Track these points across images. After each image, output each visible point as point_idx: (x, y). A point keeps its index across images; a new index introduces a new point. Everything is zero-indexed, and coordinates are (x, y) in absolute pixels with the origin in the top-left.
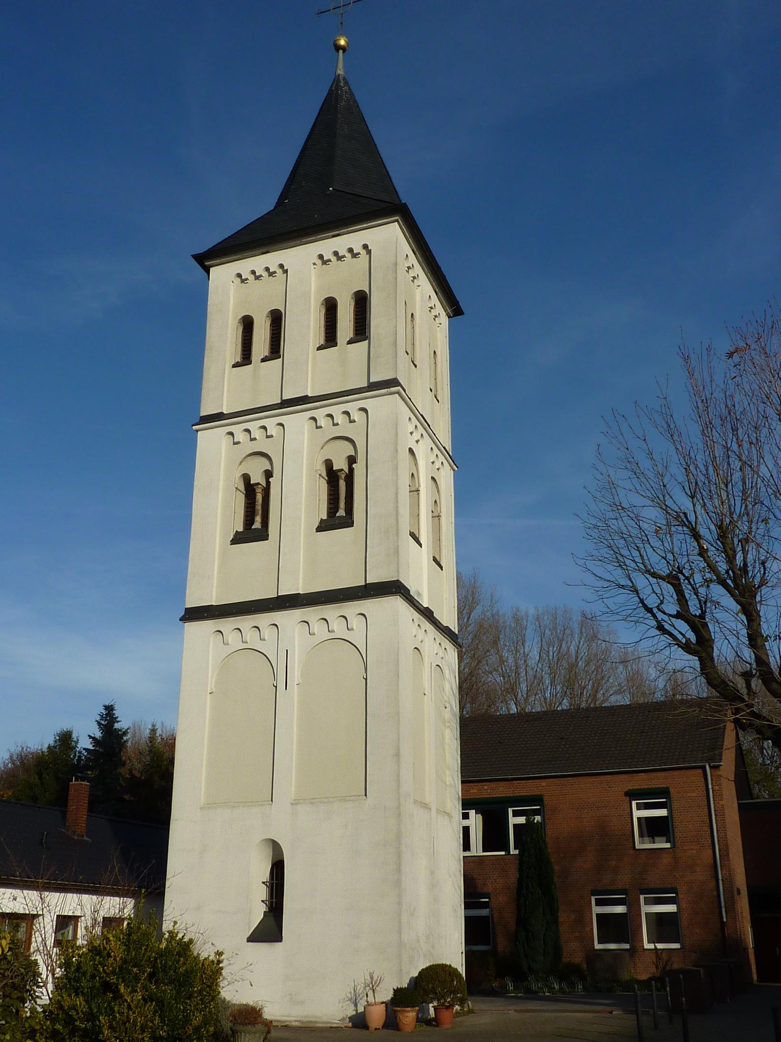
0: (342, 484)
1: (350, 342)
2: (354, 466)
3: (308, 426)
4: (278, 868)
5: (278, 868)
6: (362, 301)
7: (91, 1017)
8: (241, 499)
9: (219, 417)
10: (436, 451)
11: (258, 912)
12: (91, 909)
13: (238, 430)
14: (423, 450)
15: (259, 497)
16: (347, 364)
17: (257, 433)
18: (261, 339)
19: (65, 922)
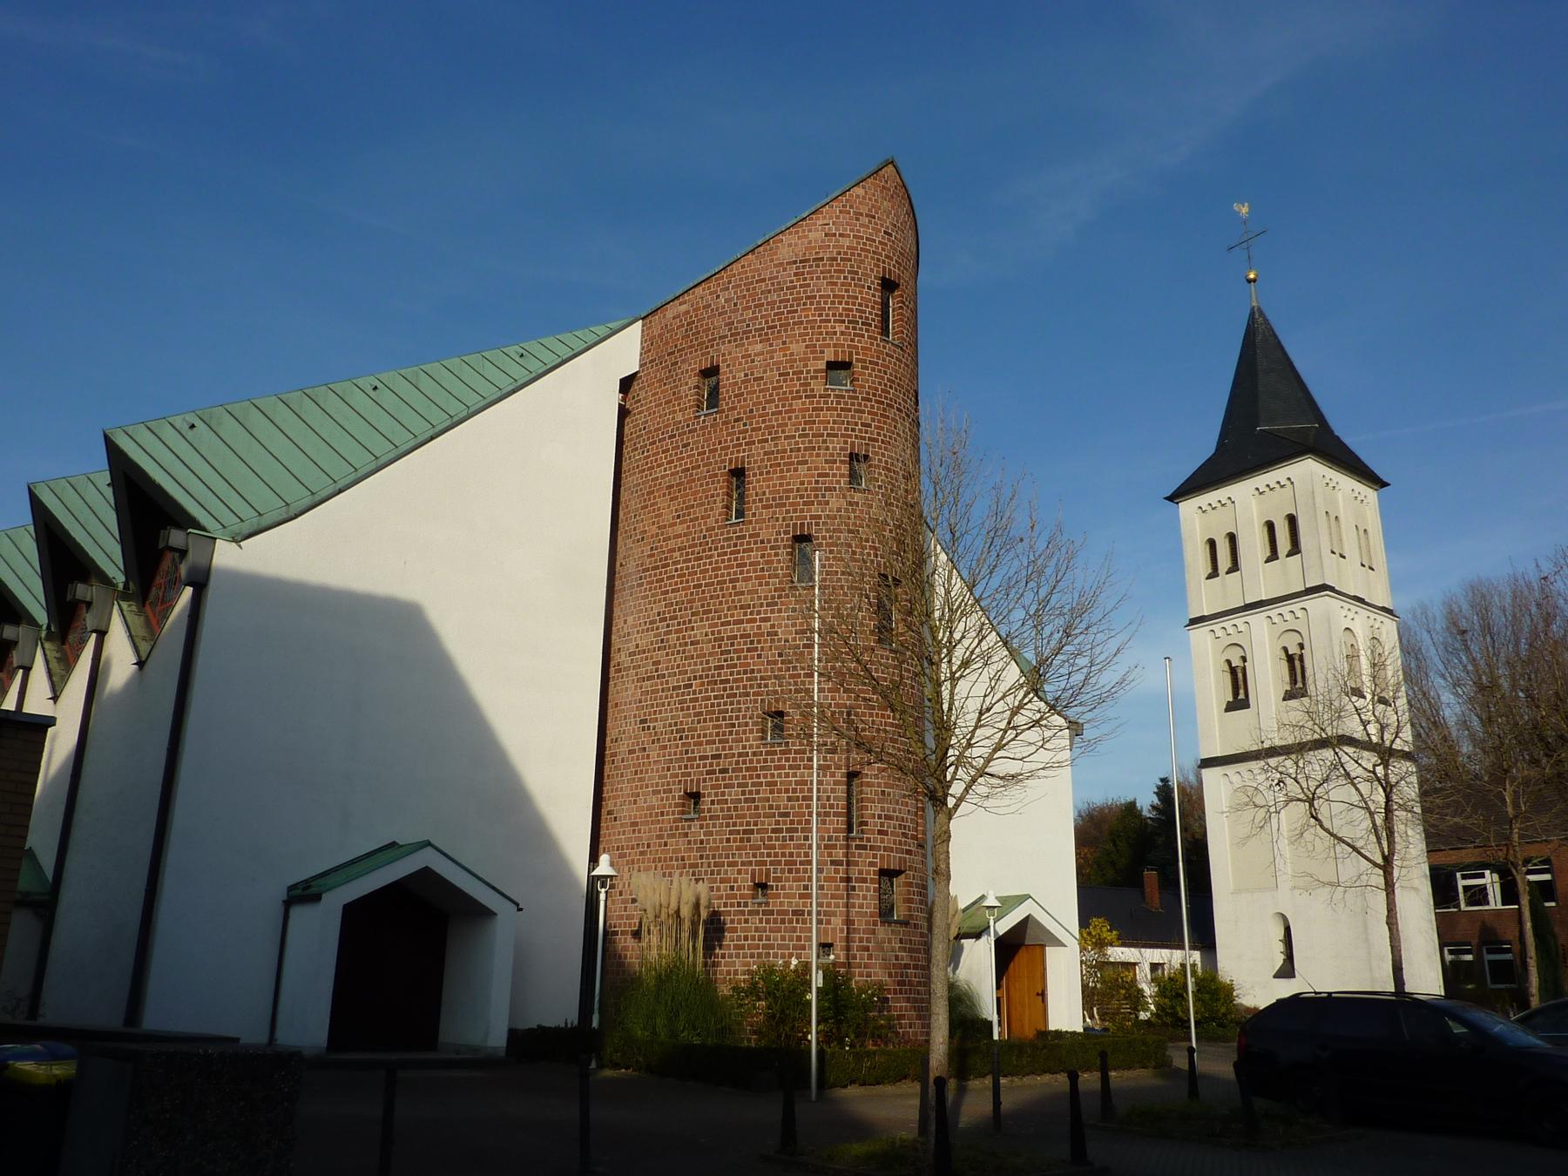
0: (1297, 663)
3: (1266, 623)
4: (1288, 930)
5: (1288, 930)
7: (1173, 1007)
8: (1228, 677)
11: (1279, 960)
12: (1171, 958)
13: (1216, 628)
15: (1240, 675)
16: (1287, 575)
17: (1231, 630)
18: (1224, 555)
19: (1154, 967)
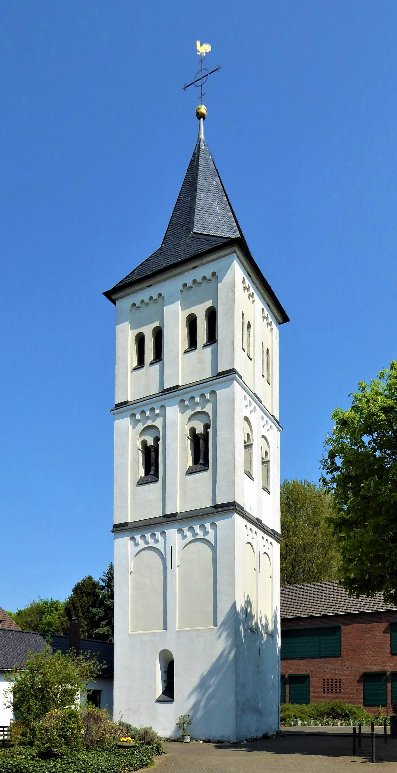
0: (202, 442)
1: (205, 346)
2: (209, 430)
6: (212, 315)
9: (125, 403)
10: (266, 418)
14: (256, 417)
